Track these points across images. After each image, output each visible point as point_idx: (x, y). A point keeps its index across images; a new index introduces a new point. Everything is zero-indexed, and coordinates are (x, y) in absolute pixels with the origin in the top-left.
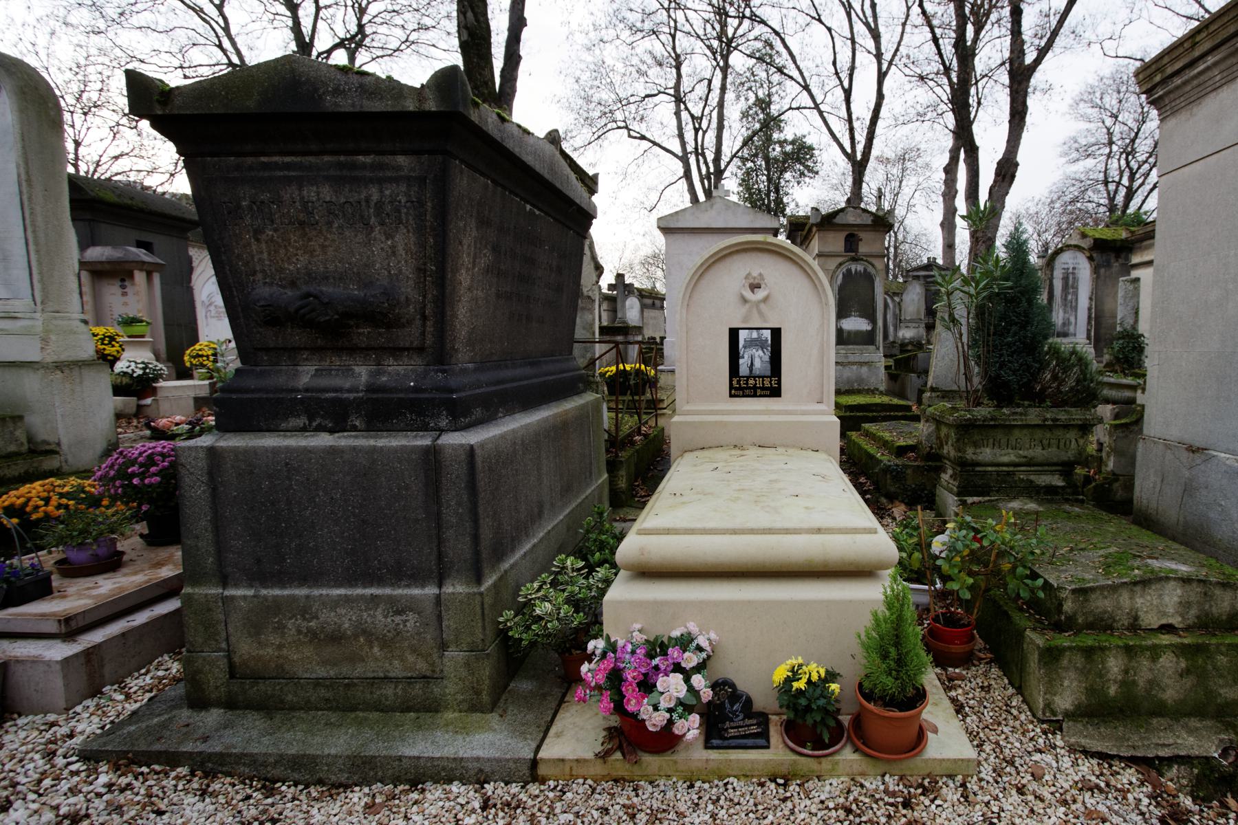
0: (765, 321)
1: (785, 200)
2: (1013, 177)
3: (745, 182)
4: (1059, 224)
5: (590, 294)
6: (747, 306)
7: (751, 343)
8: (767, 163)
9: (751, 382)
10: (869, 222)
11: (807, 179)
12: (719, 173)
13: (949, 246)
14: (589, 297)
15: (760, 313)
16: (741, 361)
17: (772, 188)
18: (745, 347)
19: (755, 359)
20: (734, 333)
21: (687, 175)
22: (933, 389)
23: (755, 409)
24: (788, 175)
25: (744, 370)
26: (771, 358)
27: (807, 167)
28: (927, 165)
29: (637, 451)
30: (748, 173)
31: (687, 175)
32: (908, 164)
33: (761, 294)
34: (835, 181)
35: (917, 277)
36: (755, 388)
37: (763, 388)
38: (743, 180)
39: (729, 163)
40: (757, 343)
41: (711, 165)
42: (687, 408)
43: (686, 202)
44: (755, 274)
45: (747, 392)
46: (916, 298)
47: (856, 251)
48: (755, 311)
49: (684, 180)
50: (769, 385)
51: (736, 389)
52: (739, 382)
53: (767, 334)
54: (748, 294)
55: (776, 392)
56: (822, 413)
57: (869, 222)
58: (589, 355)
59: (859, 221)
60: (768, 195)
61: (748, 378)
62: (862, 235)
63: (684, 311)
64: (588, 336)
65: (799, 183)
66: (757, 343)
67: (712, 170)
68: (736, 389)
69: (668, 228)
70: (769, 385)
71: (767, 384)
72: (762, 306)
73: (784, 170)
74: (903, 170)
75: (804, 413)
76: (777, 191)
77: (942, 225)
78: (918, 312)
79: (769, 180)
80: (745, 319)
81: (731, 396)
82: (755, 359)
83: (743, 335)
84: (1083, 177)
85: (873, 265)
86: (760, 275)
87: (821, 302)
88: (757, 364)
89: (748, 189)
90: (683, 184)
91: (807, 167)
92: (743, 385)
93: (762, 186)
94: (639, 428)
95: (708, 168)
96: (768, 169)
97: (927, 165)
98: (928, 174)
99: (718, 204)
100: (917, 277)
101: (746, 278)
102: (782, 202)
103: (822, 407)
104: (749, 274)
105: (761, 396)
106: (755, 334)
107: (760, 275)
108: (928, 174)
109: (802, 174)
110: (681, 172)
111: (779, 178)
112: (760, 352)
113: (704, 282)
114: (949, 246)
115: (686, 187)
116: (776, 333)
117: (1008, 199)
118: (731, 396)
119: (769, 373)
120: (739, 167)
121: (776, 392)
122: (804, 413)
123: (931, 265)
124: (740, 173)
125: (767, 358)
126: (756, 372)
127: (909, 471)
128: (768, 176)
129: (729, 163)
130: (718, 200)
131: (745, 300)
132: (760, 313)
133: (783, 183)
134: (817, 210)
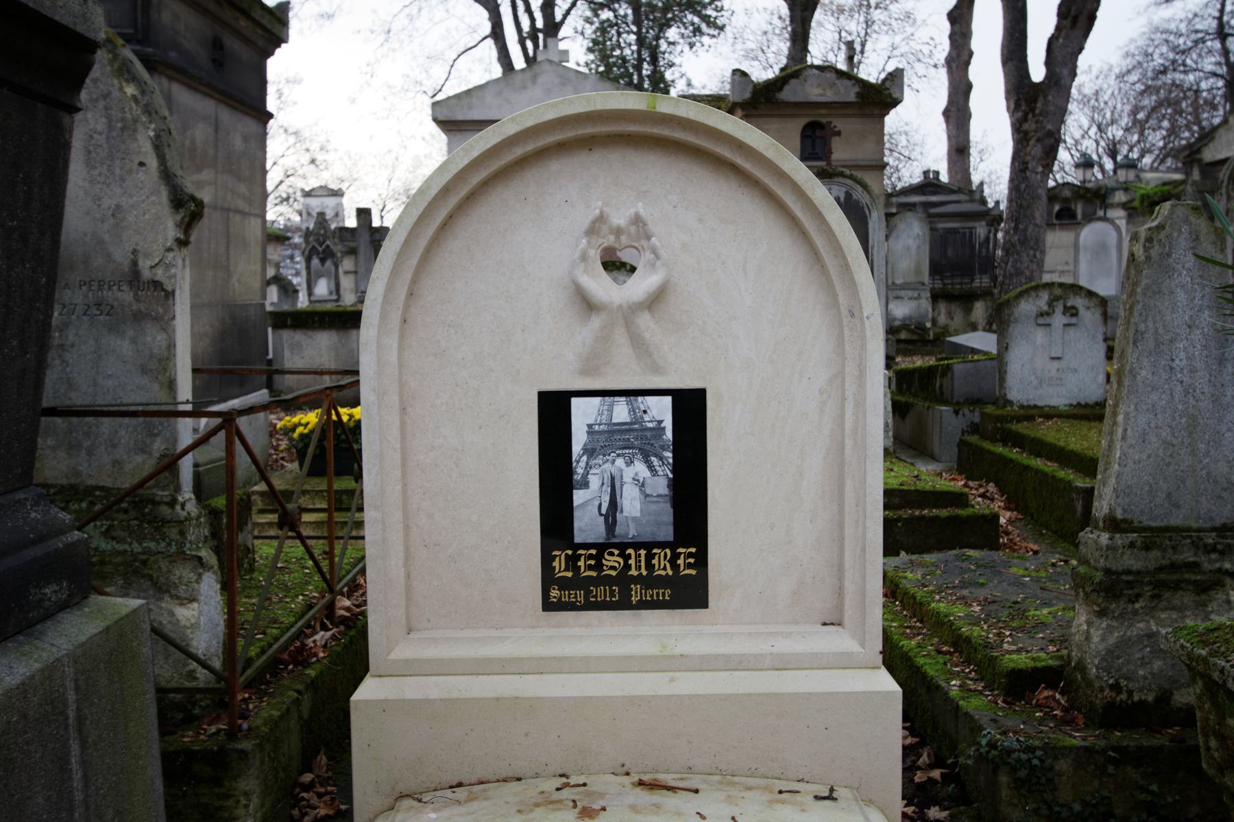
0: (656, 369)
1: (668, 75)
2: (1092, 19)
3: (599, 47)
4: (1134, 112)
5: (160, 274)
6: (596, 322)
7: (610, 439)
8: (636, 11)
9: (612, 560)
10: (852, 97)
11: (706, 39)
12: (553, 28)
13: (960, 150)
14: (157, 285)
15: (639, 344)
16: (579, 497)
17: (645, 54)
18: (590, 451)
19: (625, 491)
20: (554, 410)
21: (497, 33)
22: (1114, 525)
23: (622, 650)
24: (672, 33)
25: (587, 523)
26: (675, 484)
27: (706, 19)
28: (908, 15)
29: (313, 685)
30: (603, 29)
31: (497, 33)
32: (876, 15)
33: (640, 286)
34: (750, 45)
35: (910, 207)
36: (623, 579)
37: (650, 581)
38: (595, 42)
39: (568, 12)
40: (631, 439)
41: (538, 16)
42: (404, 651)
43: (497, 71)
44: (619, 219)
45: (600, 593)
46: (912, 244)
47: (826, 155)
48: (620, 336)
49: (490, 42)
50: (668, 567)
51: (564, 584)
52: (572, 561)
53: (661, 410)
54: (601, 285)
55: (690, 593)
56: (844, 663)
57: (852, 97)
58: (158, 446)
59: (830, 96)
60: (639, 68)
61: (601, 548)
62: (839, 124)
63: (393, 342)
64: (153, 394)
65: (692, 46)
66: (631, 439)
67: (540, 24)
68: (564, 584)
69: (454, 120)
70: (668, 567)
71: (662, 566)
72: (645, 321)
73: (664, 25)
74: (868, 23)
75: (783, 664)
76: (654, 60)
77: (946, 113)
78: (918, 271)
79: (641, 41)
80: (590, 365)
81: (548, 606)
82: (625, 491)
83: (583, 413)
84: (1183, 27)
85: (865, 187)
86: (637, 220)
87: (835, 304)
88: (631, 503)
89: (604, 57)
90: (490, 47)
91: (706, 19)
92: (584, 571)
93: (627, 52)
94: (331, 606)
95: (533, 20)
96: (638, 22)
97: (908, 15)
98: (909, 30)
99: (547, 76)
100: (910, 207)
101: (592, 230)
102: (662, 77)
103: (840, 642)
104: (601, 218)
105: (644, 605)
106: (621, 411)
107: (637, 220)
108: (909, 30)
109: (697, 31)
110: (487, 28)
111: (657, 38)
112: (640, 468)
113: (455, 245)
114: (960, 150)
115: (494, 53)
116: (690, 407)
117: (1083, 61)
118: (548, 606)
119: (667, 533)
120: (588, 21)
121: (690, 593)
122: (783, 664)
123: (930, 184)
124: (589, 30)
125: (660, 485)
126: (628, 529)
127: (1063, 765)
128: (638, 34)
129: (568, 12)
130: (546, 67)
131: (587, 305)
132: (639, 344)
133: (663, 46)
134: (744, 74)
